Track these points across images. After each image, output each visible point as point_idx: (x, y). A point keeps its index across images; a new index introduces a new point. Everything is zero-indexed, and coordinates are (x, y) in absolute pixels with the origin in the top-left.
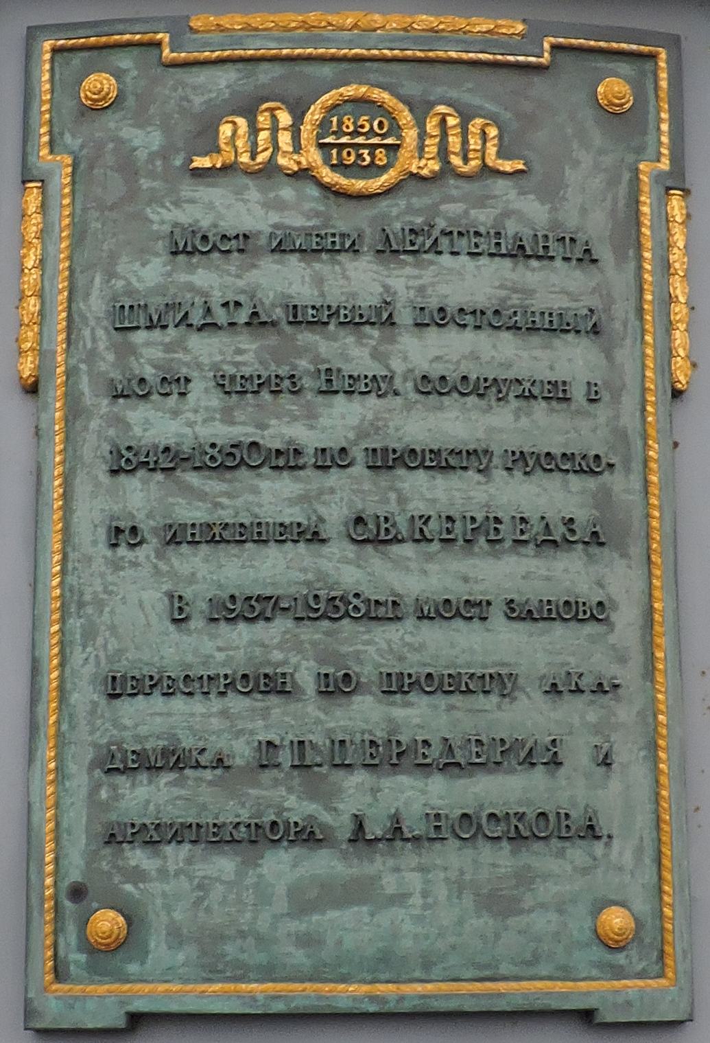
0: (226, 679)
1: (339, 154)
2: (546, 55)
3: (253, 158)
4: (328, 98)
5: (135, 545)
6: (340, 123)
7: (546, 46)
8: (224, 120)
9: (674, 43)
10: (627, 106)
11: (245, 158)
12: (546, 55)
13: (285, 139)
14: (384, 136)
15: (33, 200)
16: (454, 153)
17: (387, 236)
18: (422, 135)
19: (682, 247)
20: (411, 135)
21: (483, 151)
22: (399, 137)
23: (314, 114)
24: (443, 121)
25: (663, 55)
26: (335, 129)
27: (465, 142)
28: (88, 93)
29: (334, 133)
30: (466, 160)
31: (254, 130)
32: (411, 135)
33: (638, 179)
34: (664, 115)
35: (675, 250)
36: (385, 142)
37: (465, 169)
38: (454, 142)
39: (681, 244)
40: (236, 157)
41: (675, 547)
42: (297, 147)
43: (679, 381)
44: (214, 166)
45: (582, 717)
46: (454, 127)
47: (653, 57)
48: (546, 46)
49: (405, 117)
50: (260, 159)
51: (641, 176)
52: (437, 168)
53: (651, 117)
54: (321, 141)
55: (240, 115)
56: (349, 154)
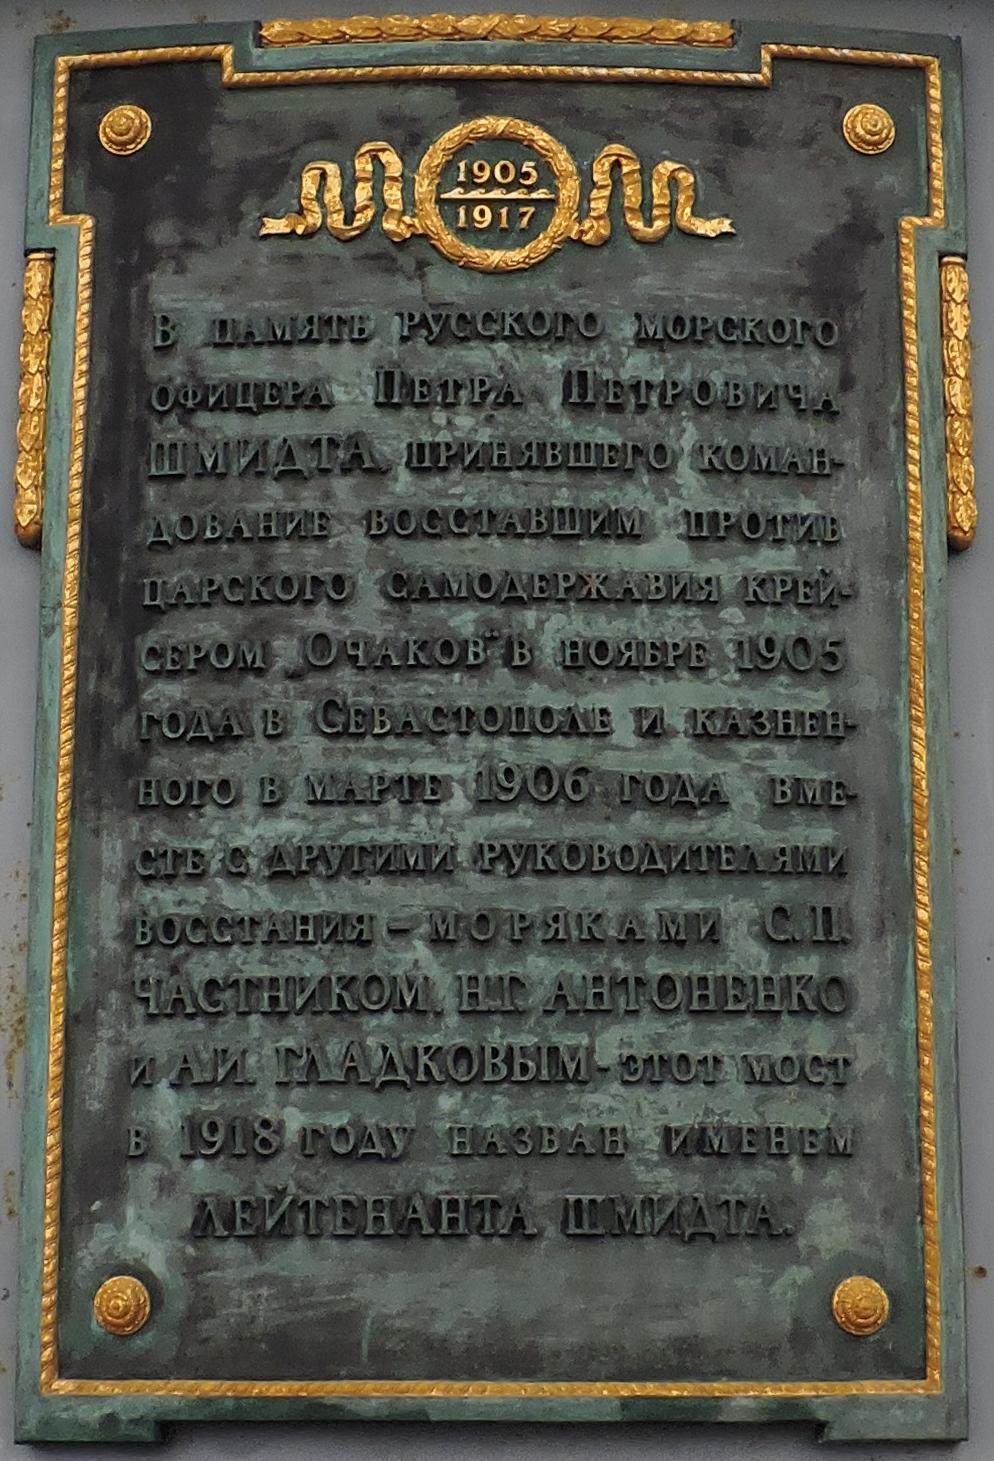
0: (309, 853)
1: (469, 214)
2: (766, 70)
3: (349, 219)
4: (452, 136)
5: (226, 806)
6: (469, 171)
7: (766, 57)
8: (307, 168)
9: (954, 55)
10: (885, 146)
11: (337, 220)
12: (766, 70)
13: (393, 194)
14: (531, 188)
15: (37, 278)
16: (631, 210)
17: (700, 1208)
18: (588, 184)
19: (962, 337)
20: (569, 190)
21: (673, 205)
22: (555, 190)
23: (434, 157)
24: (616, 165)
25: (935, 64)
26: (462, 178)
27: (646, 188)
28: (108, 130)
29: (460, 184)
30: (649, 222)
31: (350, 182)
32: (569, 190)
33: (905, 439)
34: (935, 108)
35: (953, 341)
36: (534, 196)
37: (649, 232)
38: (632, 194)
39: (961, 333)
40: (324, 216)
41: (958, 1112)
42: (410, 203)
43: (960, 528)
44: (293, 232)
45: (847, 1265)
46: (632, 172)
47: (920, 69)
48: (766, 57)
49: (563, 161)
50: (361, 220)
51: (910, 436)
52: (605, 232)
53: (921, 132)
54: (443, 196)
55: (332, 161)
56: (482, 213)
